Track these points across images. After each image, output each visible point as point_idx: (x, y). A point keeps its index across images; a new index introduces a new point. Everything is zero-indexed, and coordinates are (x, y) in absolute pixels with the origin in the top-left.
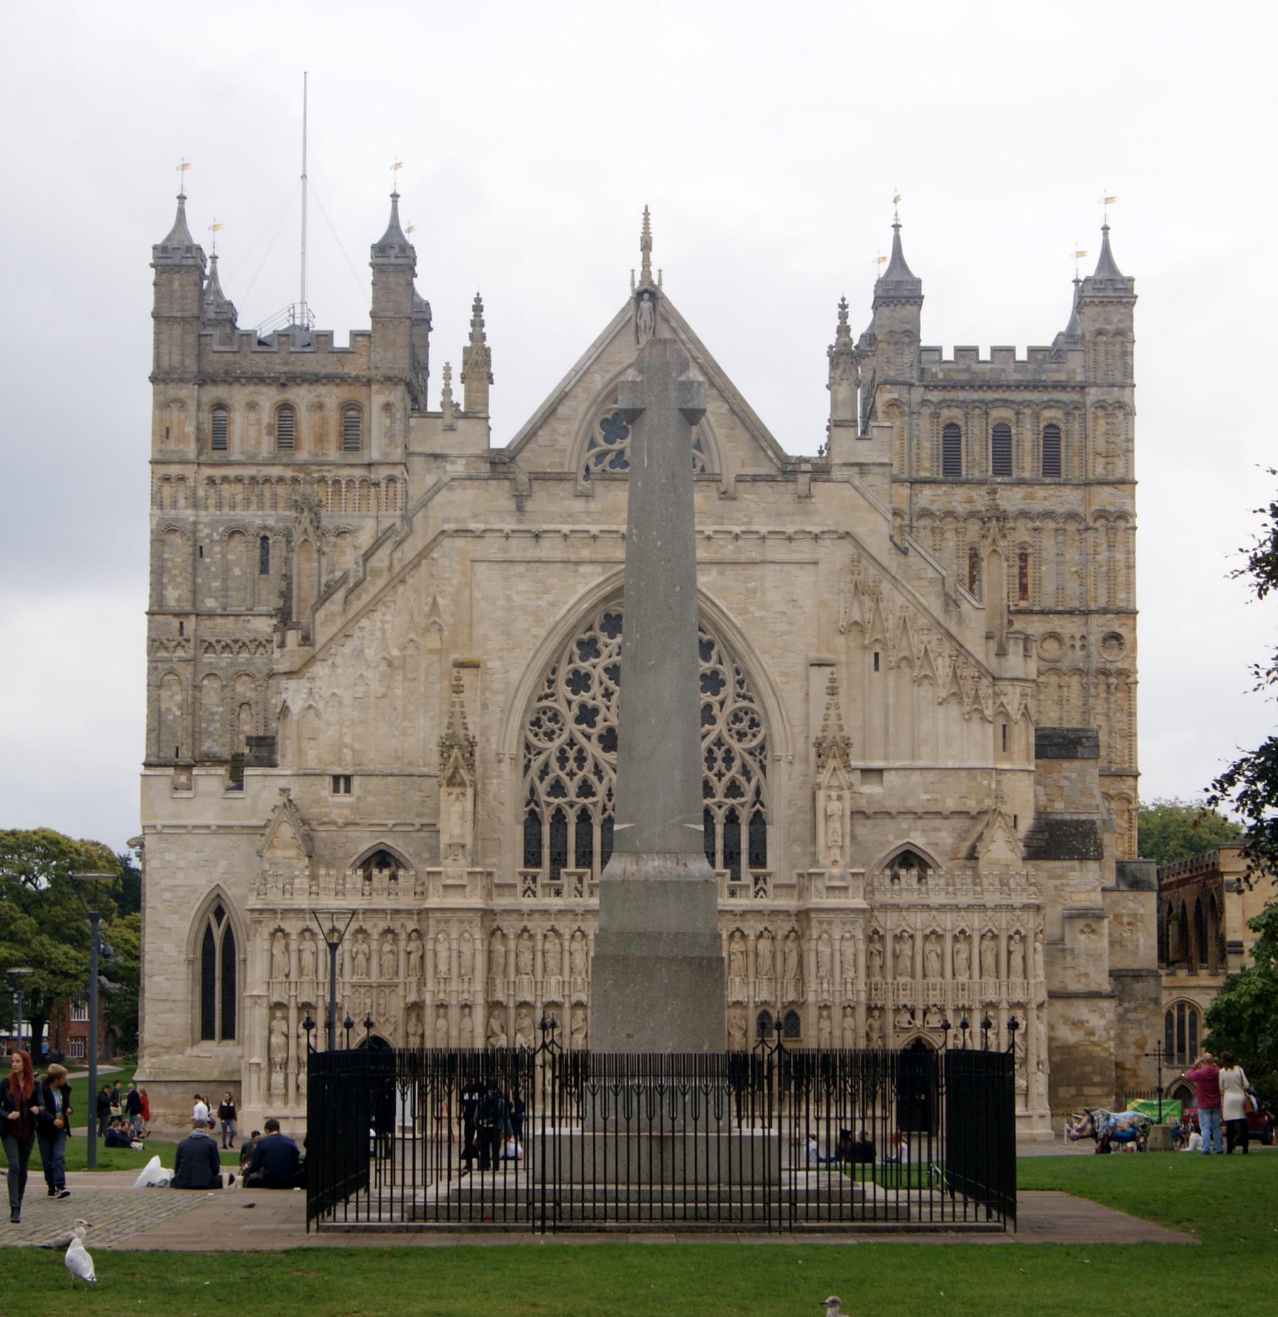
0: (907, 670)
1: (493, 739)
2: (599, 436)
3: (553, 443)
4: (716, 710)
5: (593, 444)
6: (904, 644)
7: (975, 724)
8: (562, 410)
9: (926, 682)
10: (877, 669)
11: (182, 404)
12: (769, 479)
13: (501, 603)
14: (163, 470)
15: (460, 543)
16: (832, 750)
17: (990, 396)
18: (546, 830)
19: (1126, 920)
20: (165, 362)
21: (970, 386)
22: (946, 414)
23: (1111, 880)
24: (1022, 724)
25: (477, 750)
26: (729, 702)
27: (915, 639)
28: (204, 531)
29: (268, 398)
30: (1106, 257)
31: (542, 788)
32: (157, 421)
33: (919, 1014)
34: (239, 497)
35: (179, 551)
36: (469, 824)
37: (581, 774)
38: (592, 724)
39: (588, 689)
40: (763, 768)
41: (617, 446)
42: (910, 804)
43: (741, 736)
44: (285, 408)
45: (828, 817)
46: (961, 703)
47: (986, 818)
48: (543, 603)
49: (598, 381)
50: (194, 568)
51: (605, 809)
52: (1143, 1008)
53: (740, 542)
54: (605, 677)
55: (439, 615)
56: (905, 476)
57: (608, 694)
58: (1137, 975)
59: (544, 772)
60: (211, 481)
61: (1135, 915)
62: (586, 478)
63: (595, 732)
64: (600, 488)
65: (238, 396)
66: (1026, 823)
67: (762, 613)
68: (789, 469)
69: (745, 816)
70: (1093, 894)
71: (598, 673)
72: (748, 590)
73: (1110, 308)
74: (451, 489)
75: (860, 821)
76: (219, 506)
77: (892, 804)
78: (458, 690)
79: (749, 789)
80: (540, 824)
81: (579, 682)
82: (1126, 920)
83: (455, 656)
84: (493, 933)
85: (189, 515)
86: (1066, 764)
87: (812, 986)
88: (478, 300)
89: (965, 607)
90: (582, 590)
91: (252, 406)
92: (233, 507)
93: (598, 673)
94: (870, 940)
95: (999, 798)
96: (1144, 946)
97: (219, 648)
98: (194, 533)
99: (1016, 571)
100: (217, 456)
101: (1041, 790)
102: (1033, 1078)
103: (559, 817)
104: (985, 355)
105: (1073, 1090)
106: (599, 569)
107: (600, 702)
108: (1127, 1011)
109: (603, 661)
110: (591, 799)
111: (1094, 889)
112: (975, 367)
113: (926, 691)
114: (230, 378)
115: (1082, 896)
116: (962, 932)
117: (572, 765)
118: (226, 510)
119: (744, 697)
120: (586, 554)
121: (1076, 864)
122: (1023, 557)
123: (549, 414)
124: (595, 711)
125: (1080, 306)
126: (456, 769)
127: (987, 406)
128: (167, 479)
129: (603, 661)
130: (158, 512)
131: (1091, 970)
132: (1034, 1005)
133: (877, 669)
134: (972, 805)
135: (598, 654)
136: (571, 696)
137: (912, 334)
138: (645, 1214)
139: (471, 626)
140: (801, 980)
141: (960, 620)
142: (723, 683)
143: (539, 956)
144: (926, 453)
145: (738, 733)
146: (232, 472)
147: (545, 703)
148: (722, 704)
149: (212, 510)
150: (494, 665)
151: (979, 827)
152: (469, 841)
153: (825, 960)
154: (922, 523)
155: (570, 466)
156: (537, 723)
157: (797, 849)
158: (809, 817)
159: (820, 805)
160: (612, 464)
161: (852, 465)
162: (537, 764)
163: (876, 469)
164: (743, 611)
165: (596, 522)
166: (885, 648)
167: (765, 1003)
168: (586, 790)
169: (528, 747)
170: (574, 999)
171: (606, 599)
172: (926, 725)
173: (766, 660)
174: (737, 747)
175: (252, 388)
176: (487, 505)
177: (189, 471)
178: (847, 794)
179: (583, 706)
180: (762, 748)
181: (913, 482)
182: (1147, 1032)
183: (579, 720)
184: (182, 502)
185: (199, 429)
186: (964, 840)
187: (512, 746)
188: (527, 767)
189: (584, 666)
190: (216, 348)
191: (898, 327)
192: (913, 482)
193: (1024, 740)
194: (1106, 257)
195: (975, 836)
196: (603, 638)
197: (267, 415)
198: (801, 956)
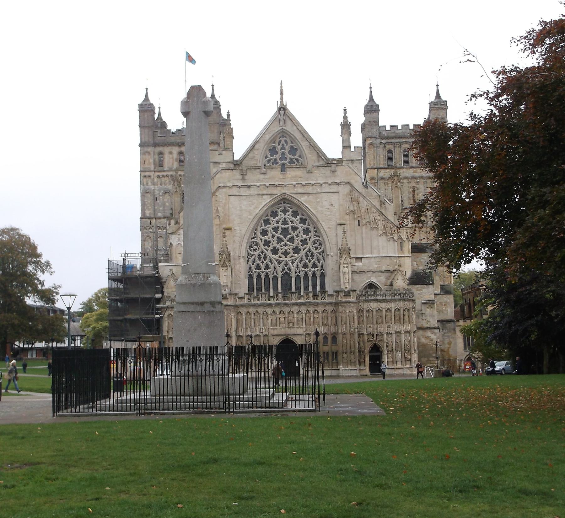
0: (369, 226)
1: (237, 252)
2: (269, 154)
3: (254, 157)
4: (308, 241)
5: (266, 157)
6: (368, 217)
7: (391, 242)
8: (256, 147)
9: (375, 229)
10: (359, 225)
11: (149, 153)
12: (323, 166)
13: (238, 208)
14: (143, 174)
15: (224, 190)
16: (344, 252)
17: (402, 140)
18: (255, 280)
19: (443, 304)
20: (143, 140)
21: (395, 137)
22: (388, 147)
23: (438, 291)
24: (407, 242)
25: (231, 255)
26: (312, 237)
27: (371, 215)
28: (157, 192)
29: (175, 150)
30: (438, 95)
31: (253, 267)
32: (141, 159)
33: (375, 336)
34: (167, 181)
35: (149, 199)
36: (229, 279)
37: (265, 262)
38: (269, 246)
39: (267, 235)
40: (324, 258)
41: (274, 158)
42: (371, 268)
43: (316, 248)
44: (181, 153)
45: (344, 273)
46: (387, 235)
47: (396, 272)
48: (252, 208)
49: (267, 137)
50: (154, 204)
51: (273, 273)
52: (450, 332)
53: (314, 186)
54: (272, 231)
55: (219, 213)
56: (375, 167)
57: (273, 236)
58: (448, 321)
59: (254, 262)
60: (159, 177)
61: (446, 302)
62: (264, 168)
63: (292, 254)
64: (269, 171)
65: (166, 150)
66: (409, 274)
67: (321, 209)
68: (330, 163)
69: (318, 274)
70: (431, 296)
71: (270, 230)
72: (317, 202)
73: (440, 111)
74: (221, 173)
75: (355, 275)
76: (161, 184)
77: (365, 269)
78: (224, 236)
79: (319, 265)
80: (253, 278)
81: (264, 233)
82: (443, 304)
83: (224, 226)
84: (238, 313)
85: (152, 187)
86: (423, 254)
87: (340, 327)
88: (228, 113)
89: (387, 205)
90: (264, 203)
91: (171, 153)
92: (166, 184)
93: (270, 230)
94: (359, 312)
95: (400, 266)
96: (450, 312)
97: (162, 228)
98: (154, 193)
99: (412, 195)
100: (160, 169)
101: (415, 263)
102: (413, 355)
103: (259, 276)
104: (400, 127)
105: (426, 359)
106: (269, 196)
107: (271, 239)
108: (444, 333)
109: (272, 226)
110: (269, 270)
111: (431, 294)
112: (397, 132)
113: (375, 232)
114: (164, 145)
115: (428, 296)
116: (388, 309)
117: (262, 259)
118: (163, 185)
119: (317, 236)
120: (265, 192)
121: (425, 286)
122: (414, 191)
123: (252, 148)
124: (270, 242)
125: (431, 110)
126: (224, 262)
127: (400, 144)
128: (145, 177)
129: (272, 226)
130: (142, 187)
131: (431, 320)
132: (412, 332)
133: (359, 225)
134: (391, 268)
135: (270, 224)
136: (262, 237)
137: (377, 122)
138: (128, 408)
139: (229, 216)
140: (336, 325)
141: (386, 209)
142: (310, 232)
143: (253, 320)
144: (382, 159)
145: (315, 247)
146: (165, 174)
147: (253, 240)
148: (310, 238)
149: (159, 186)
150: (237, 228)
151: (394, 275)
152: (229, 284)
153: (344, 319)
154: (381, 181)
155: (260, 164)
156: (251, 246)
157: (335, 284)
158: (338, 274)
159: (341, 270)
160: (273, 163)
161: (349, 160)
162: (251, 259)
163: (357, 161)
164: (316, 209)
165: (268, 182)
166: (361, 219)
167: (325, 333)
168: (267, 267)
169: (248, 254)
170: (264, 334)
171: (272, 206)
172: (375, 244)
173: (323, 224)
174: (315, 252)
175: (170, 148)
176: (234, 178)
177: (152, 174)
178: (350, 266)
179: (265, 241)
180: (323, 252)
181: (378, 169)
182: (451, 340)
183: (264, 245)
184: (150, 183)
185: (154, 161)
186: (389, 279)
187: (243, 254)
188: (248, 260)
189: (266, 228)
190: (159, 135)
191: (372, 120)
192: (378, 169)
193: (407, 246)
194: (438, 95)
195: (392, 278)
196: (271, 218)
197: (175, 155)
198: (336, 318)
